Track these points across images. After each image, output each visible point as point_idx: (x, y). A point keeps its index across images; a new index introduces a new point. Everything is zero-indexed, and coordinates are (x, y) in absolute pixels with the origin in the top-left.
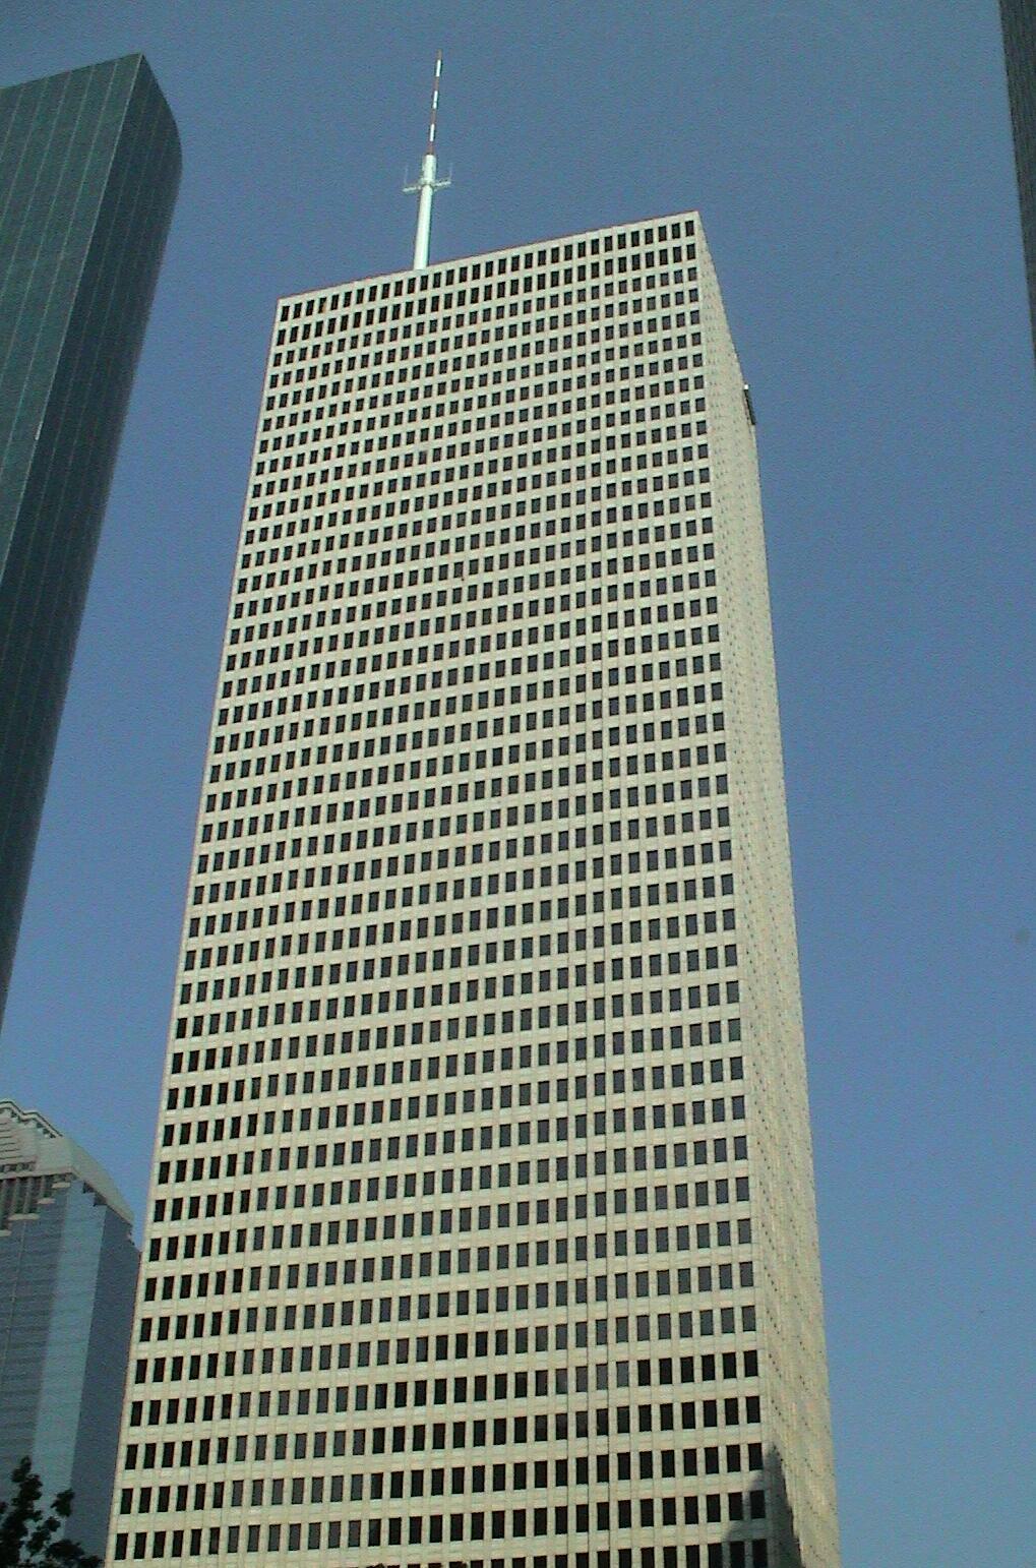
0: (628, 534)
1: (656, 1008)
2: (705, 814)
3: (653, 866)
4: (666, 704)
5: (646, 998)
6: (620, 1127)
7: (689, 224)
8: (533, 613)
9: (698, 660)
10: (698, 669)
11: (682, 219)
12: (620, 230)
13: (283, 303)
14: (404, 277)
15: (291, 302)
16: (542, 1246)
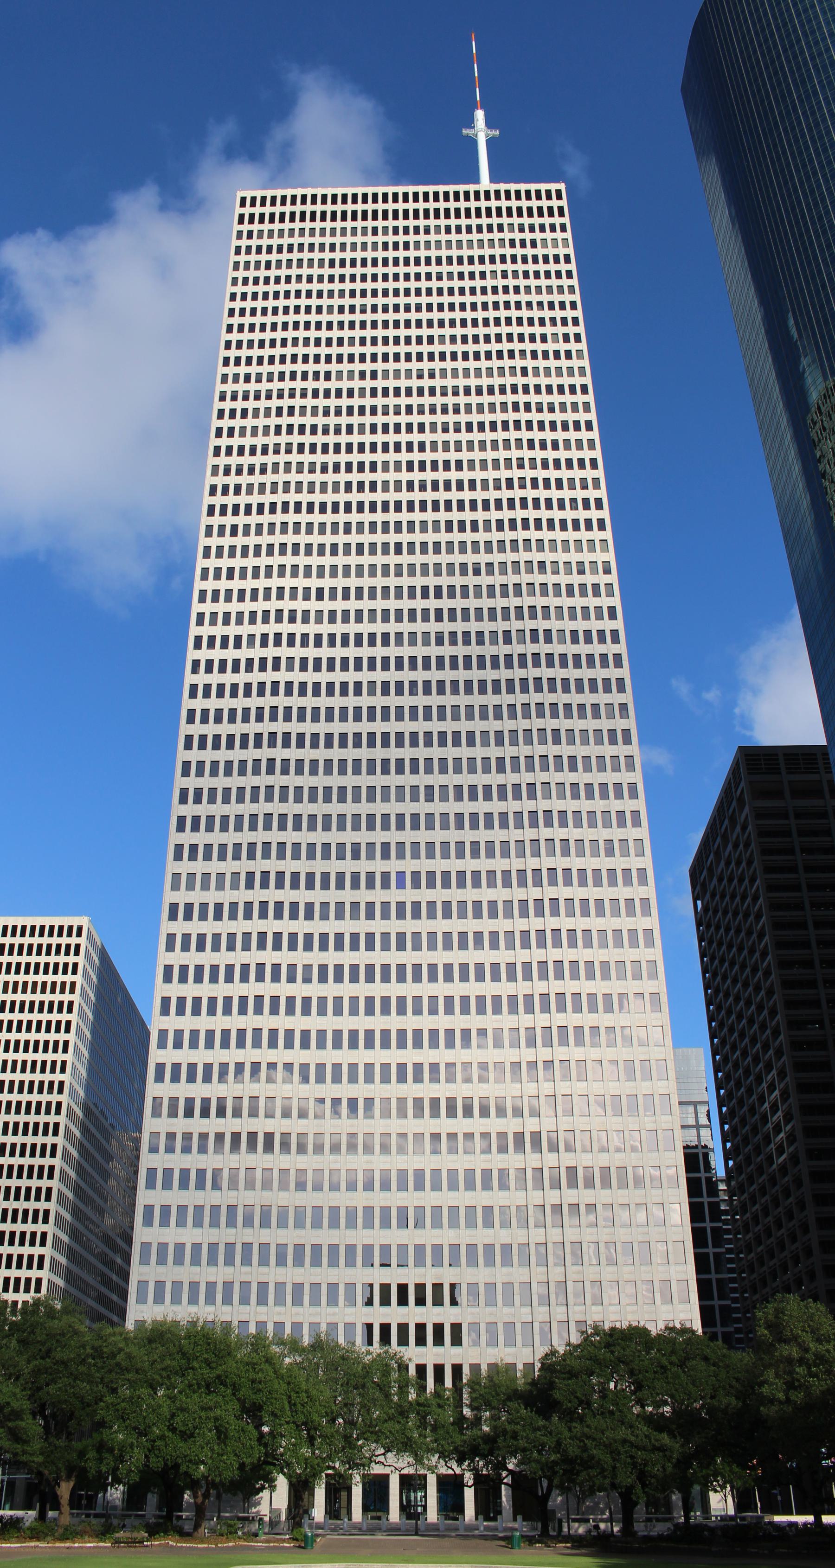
0: (287, 484)
1: (297, 827)
2: (330, 710)
3: (219, 712)
4: (292, 620)
5: (290, 819)
6: (265, 885)
7: (559, 192)
8: (271, 532)
9: (281, 590)
10: (280, 596)
11: (553, 187)
12: (344, 190)
13: (240, 194)
14: (471, 188)
15: (248, 194)
16: (232, 936)
